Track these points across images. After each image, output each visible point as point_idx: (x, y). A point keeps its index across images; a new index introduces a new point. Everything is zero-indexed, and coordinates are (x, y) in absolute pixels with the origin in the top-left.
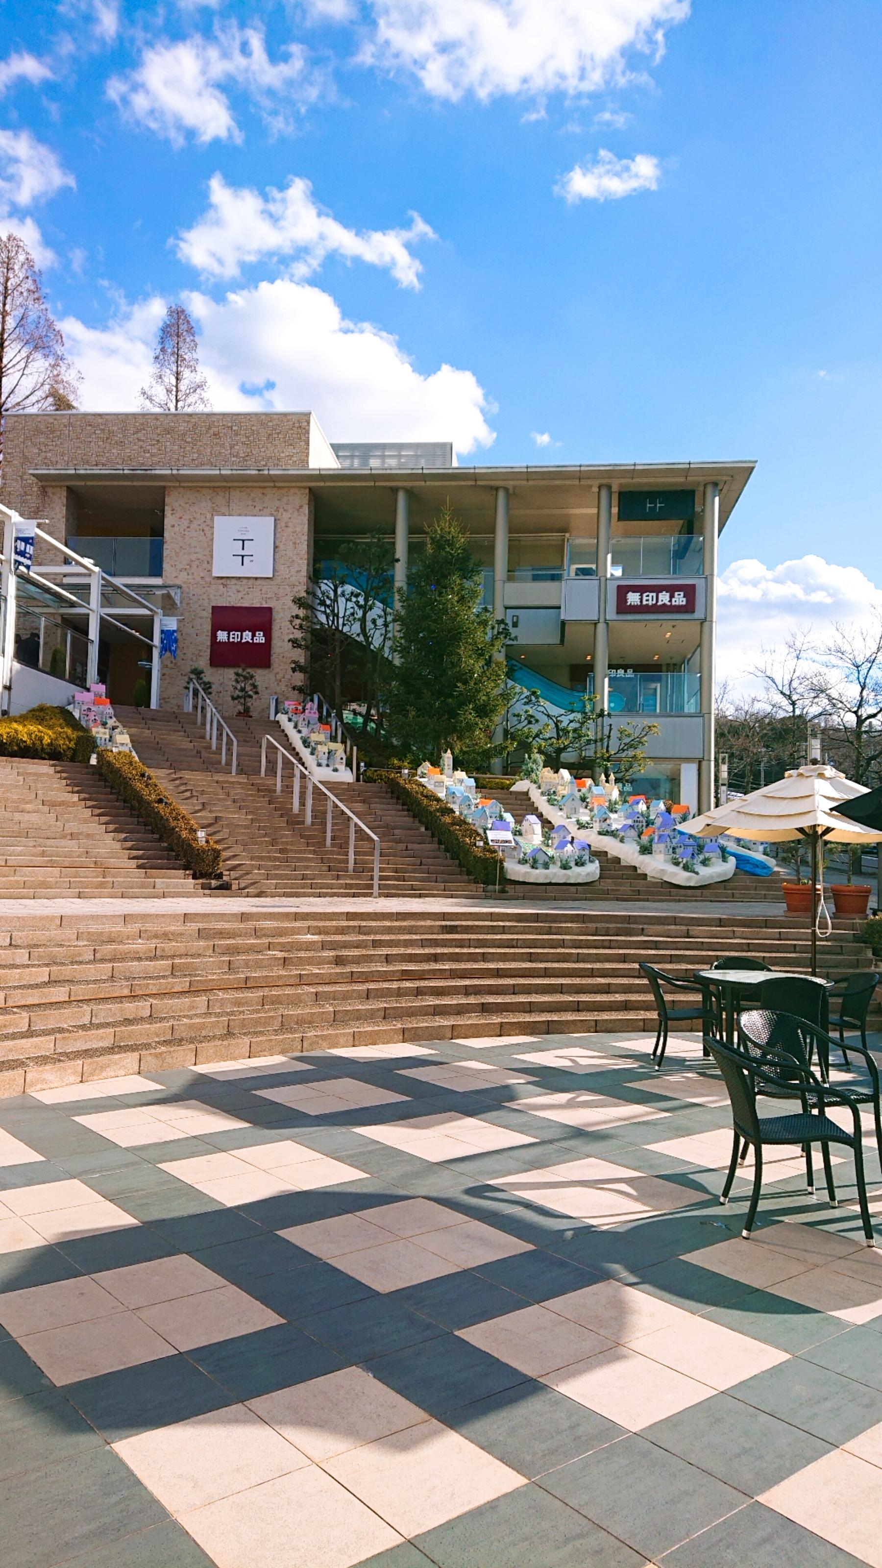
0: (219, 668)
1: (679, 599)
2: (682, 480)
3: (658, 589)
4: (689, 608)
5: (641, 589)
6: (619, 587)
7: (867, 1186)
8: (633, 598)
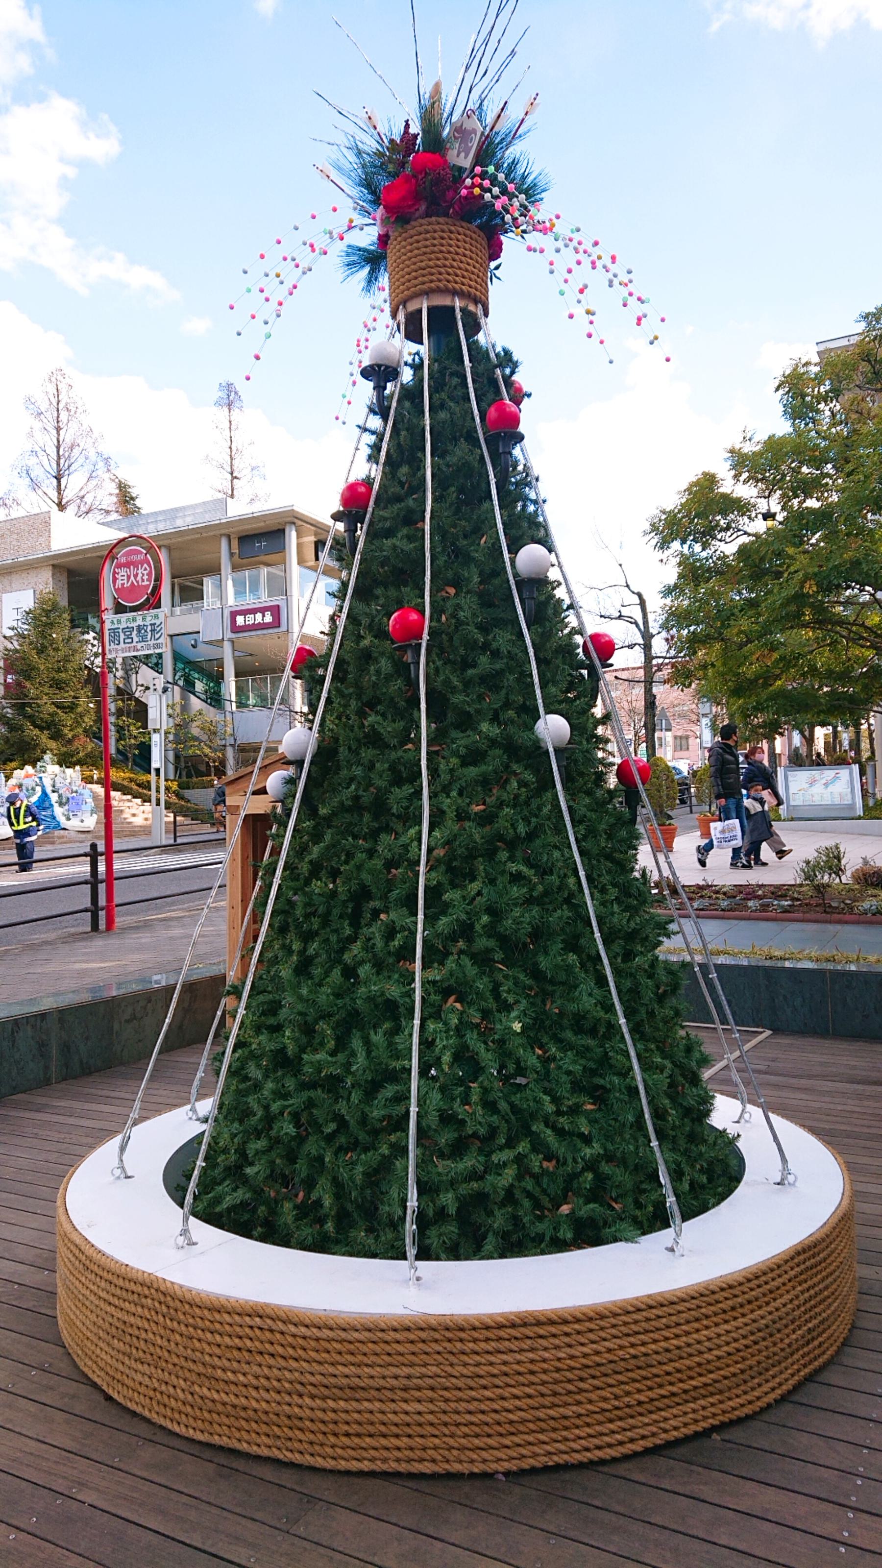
0: (85, 997)
1: (268, 618)
2: (262, 524)
3: (253, 611)
4: (276, 623)
5: (244, 613)
6: (232, 612)
7: (115, 855)
8: (240, 620)
